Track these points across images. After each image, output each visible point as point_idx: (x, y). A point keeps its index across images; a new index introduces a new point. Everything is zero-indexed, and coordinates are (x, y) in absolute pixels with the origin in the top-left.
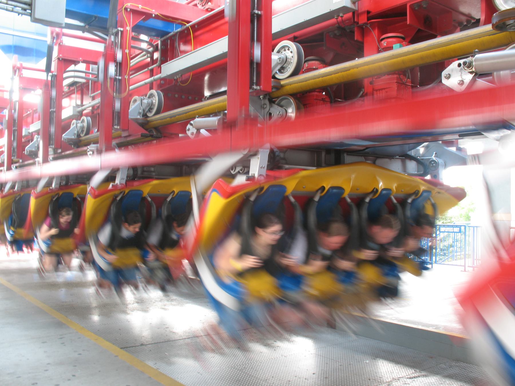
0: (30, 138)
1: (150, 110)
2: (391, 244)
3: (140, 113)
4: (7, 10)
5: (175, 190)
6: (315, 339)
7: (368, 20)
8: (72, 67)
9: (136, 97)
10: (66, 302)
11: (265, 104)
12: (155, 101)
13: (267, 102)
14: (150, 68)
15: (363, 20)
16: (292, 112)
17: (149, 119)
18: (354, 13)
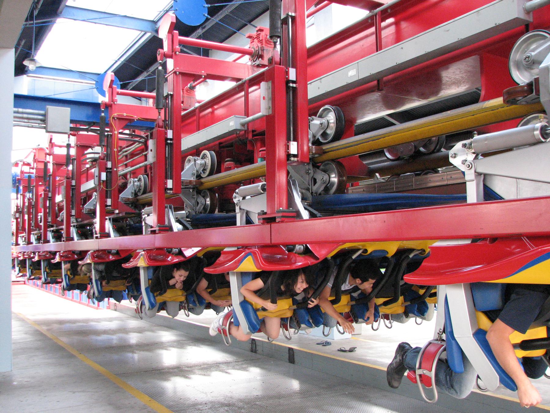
0: (88, 196)
1: (204, 170)
2: (380, 305)
3: (193, 174)
4: (28, 127)
5: (12, 242)
6: (262, 368)
7: (253, 137)
8: (90, 150)
9: (190, 157)
10: (174, 401)
11: (309, 169)
12: (208, 161)
13: (311, 167)
14: (125, 163)
15: (250, 137)
16: (335, 177)
17: (203, 180)
18: (378, 81)
